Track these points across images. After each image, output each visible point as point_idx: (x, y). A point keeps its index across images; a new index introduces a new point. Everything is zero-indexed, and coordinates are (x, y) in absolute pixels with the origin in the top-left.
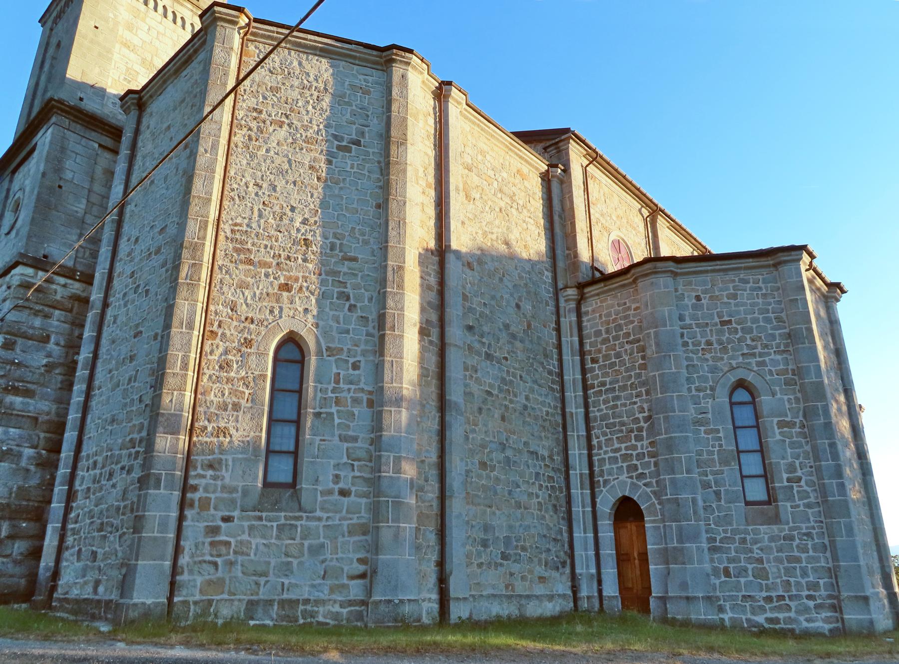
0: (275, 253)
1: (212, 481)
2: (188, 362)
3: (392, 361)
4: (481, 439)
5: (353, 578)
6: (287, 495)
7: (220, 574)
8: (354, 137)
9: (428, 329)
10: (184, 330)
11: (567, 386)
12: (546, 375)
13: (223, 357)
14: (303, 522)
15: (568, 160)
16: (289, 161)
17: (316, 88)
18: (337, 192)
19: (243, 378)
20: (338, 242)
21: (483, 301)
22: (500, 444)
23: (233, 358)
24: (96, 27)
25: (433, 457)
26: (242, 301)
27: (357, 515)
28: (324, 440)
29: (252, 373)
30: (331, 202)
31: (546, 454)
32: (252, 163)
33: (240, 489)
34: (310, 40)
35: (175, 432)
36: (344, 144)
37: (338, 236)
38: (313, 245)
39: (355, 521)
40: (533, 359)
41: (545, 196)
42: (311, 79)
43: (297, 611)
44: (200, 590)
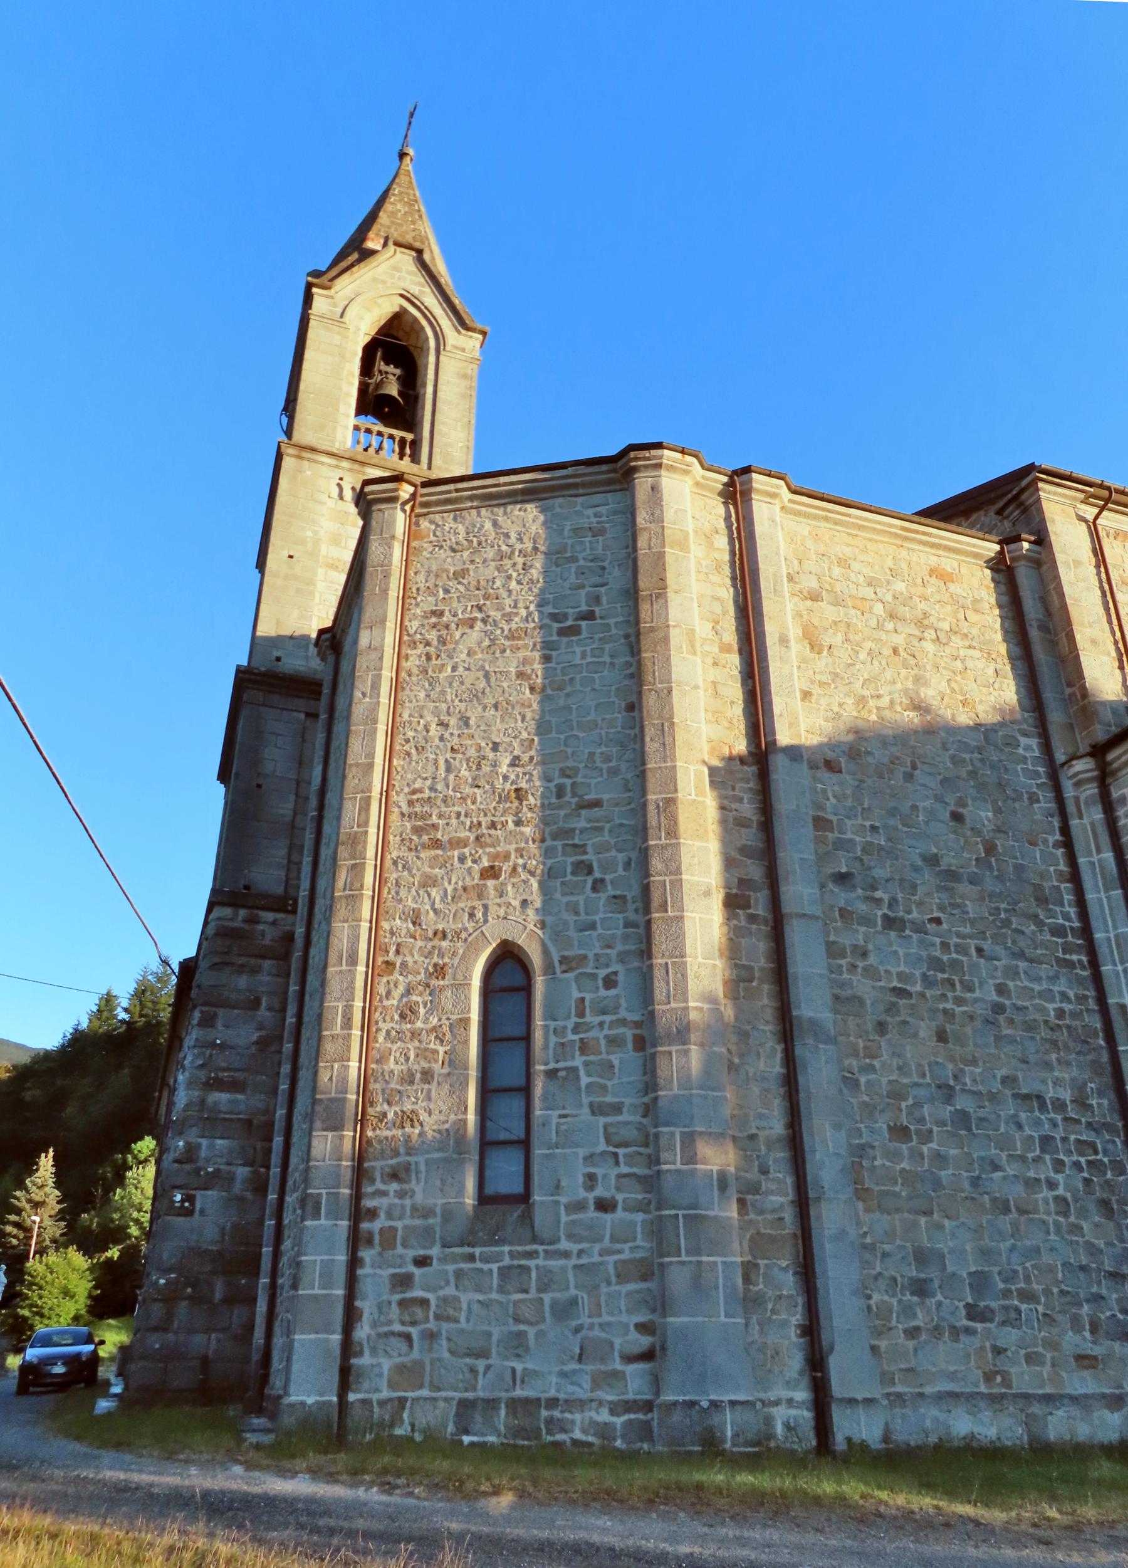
0: (472, 822)
1: (397, 1201)
2: (352, 1014)
3: (667, 964)
4: (890, 1082)
5: (630, 1359)
6: (516, 1215)
7: (416, 1354)
8: (584, 608)
9: (743, 896)
10: (344, 967)
11: (1103, 951)
12: (1048, 937)
13: (405, 1000)
14: (540, 1261)
15: (1043, 521)
16: (487, 676)
17: (520, 551)
18: (561, 702)
19: (434, 1029)
20: (568, 782)
21: (868, 824)
22: (939, 1087)
23: (419, 999)
24: (291, 557)
25: (777, 1126)
26: (428, 907)
27: (631, 1244)
28: (565, 1116)
29: (448, 1019)
30: (553, 720)
31: (1067, 1095)
32: (432, 693)
33: (438, 1210)
34: (505, 484)
35: (336, 1126)
36: (569, 623)
37: (568, 772)
38: (530, 797)
39: (625, 1256)
40: (1006, 910)
41: (1005, 599)
42: (513, 539)
43: (538, 1420)
44: (389, 1381)
